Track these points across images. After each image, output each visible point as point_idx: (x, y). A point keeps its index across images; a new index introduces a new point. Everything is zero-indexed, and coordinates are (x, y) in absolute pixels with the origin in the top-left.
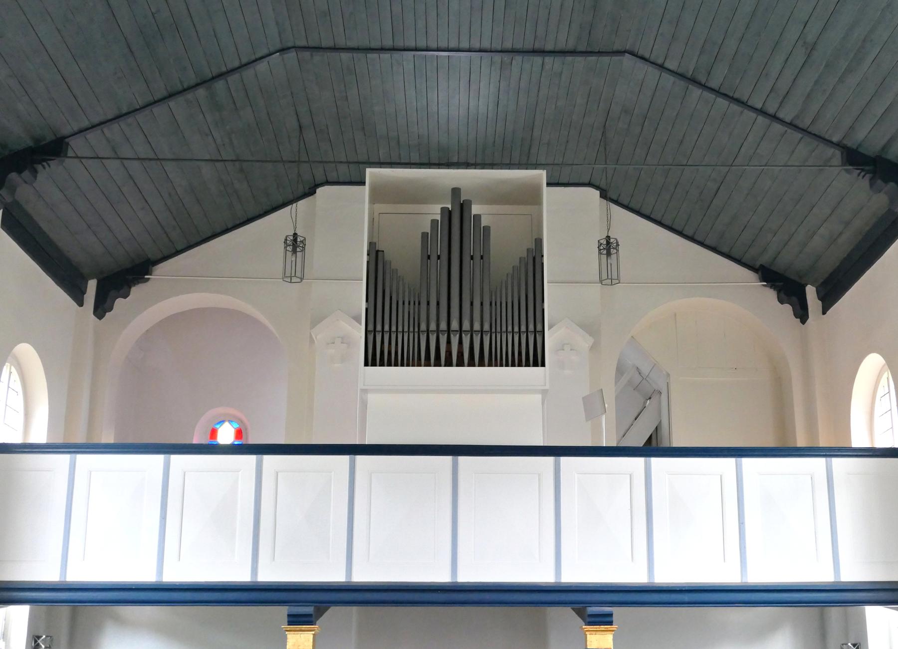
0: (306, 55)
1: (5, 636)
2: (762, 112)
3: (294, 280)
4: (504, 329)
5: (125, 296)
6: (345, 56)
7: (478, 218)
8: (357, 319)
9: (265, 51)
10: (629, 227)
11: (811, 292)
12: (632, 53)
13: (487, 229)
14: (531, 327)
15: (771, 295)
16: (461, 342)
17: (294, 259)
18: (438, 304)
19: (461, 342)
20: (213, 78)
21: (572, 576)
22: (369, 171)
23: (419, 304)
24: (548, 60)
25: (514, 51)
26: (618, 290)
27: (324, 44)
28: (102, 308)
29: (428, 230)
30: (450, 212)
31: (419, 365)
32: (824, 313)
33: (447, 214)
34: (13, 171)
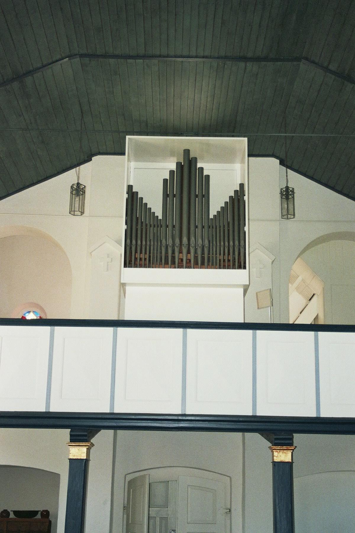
0: (87, 60)
6: (112, 61)
7: (202, 169)
8: (119, 243)
9: (58, 57)
10: (298, 182)
12: (307, 59)
13: (208, 177)
20: (24, 74)
21: (265, 410)
22: (127, 137)
24: (249, 65)
25: (226, 57)
26: (290, 224)
27: (98, 53)
29: (168, 177)
34: (28, 320)
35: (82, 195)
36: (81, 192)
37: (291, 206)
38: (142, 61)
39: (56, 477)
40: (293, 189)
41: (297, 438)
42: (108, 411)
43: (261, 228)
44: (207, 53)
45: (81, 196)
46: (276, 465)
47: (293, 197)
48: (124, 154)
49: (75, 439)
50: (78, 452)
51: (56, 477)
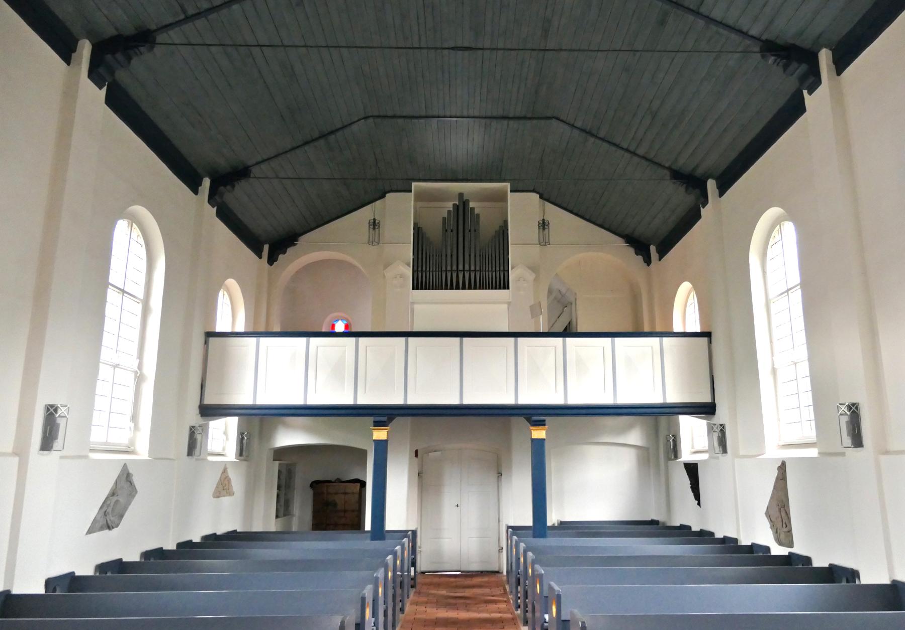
0: (379, 120)
2: (627, 150)
5: (284, 253)
6: (400, 121)
7: (473, 209)
8: (408, 265)
10: (555, 214)
11: (653, 249)
13: (478, 215)
14: (502, 268)
15: (631, 251)
21: (524, 400)
22: (414, 184)
24: (511, 122)
28: (272, 260)
29: (446, 215)
33: (456, 207)
41: (548, 419)
44: (477, 114)
48: (410, 191)
49: (378, 424)
50: (380, 434)
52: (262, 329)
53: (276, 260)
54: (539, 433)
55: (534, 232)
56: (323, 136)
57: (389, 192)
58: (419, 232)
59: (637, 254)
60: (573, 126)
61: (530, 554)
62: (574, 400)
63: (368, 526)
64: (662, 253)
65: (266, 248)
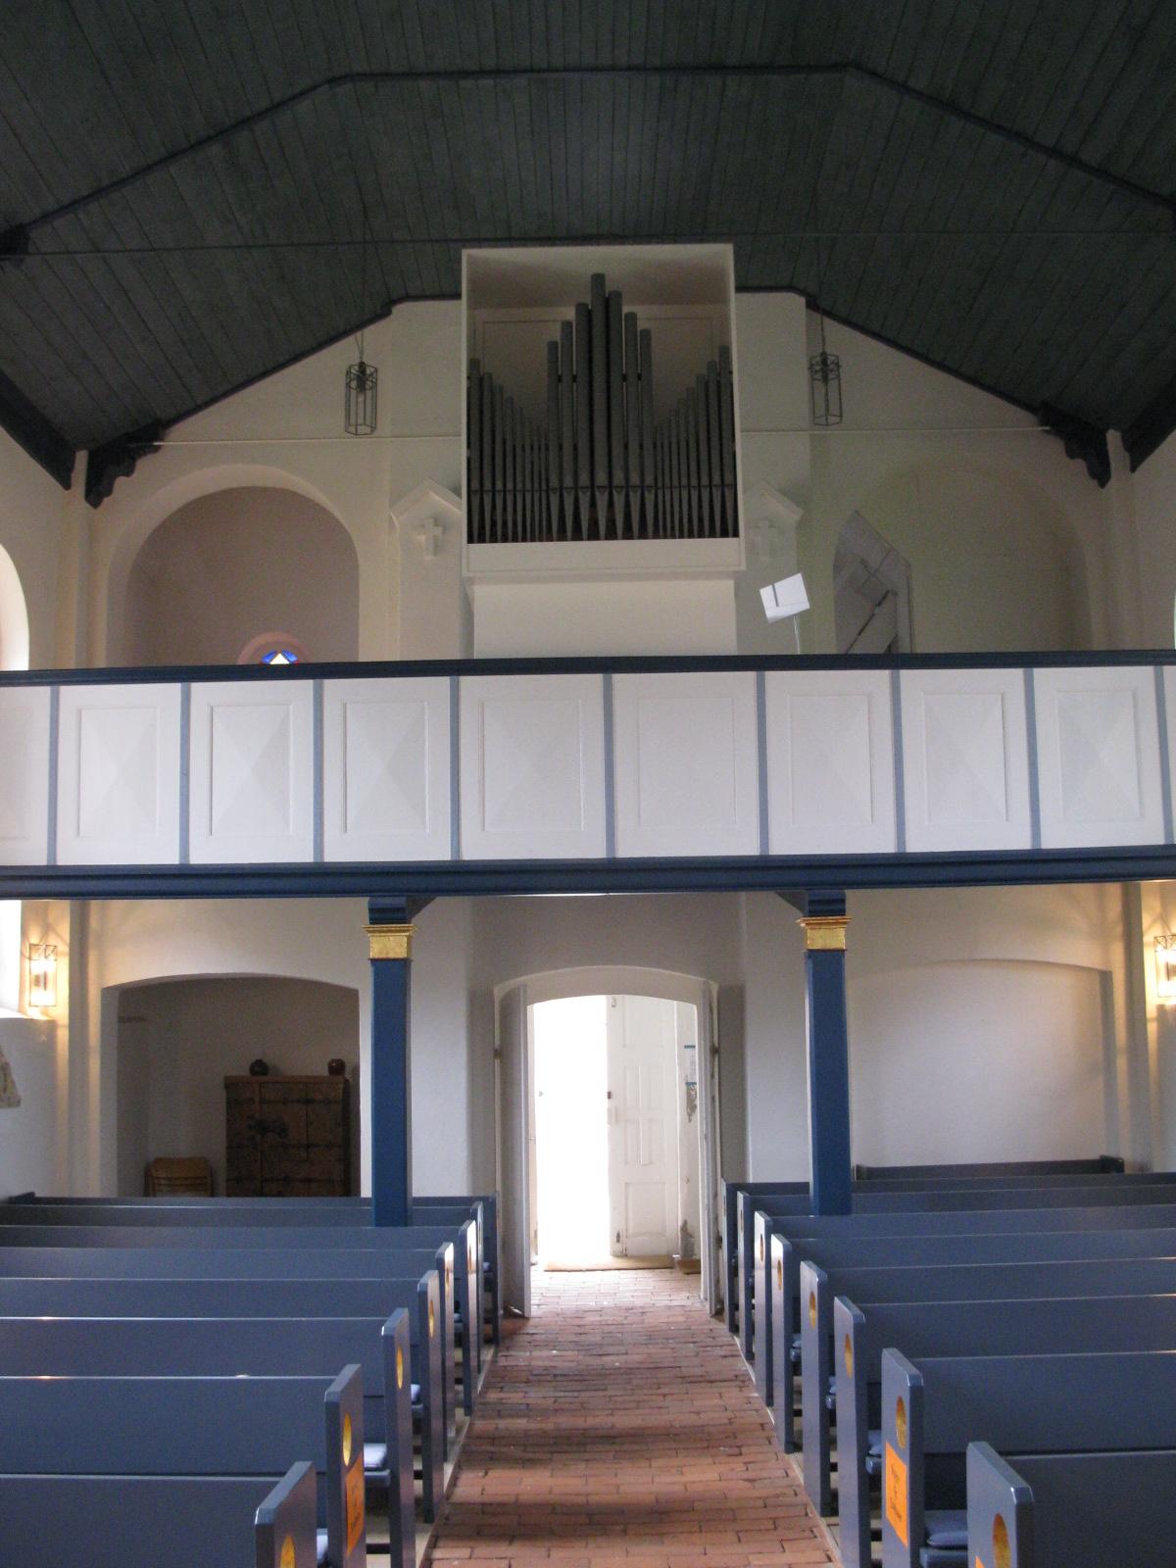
1: (790, 1565)
2: (1054, 152)
3: (362, 429)
4: (676, 483)
5: (129, 472)
6: (423, 85)
7: (632, 317)
8: (457, 491)
11: (1113, 439)
13: (646, 333)
14: (717, 479)
15: (1055, 447)
16: (611, 504)
17: (361, 399)
18: (575, 448)
19: (611, 504)
20: (233, 126)
21: (787, 843)
22: (467, 254)
23: (547, 449)
25: (680, 69)
28: (96, 492)
29: (557, 336)
30: (590, 313)
31: (550, 539)
32: (1133, 469)
33: (585, 313)
35: (371, 388)
36: (370, 384)
37: (833, 395)
38: (491, 81)
39: (351, 996)
40: (837, 357)
41: (852, 896)
42: (448, 858)
43: (763, 457)
45: (369, 393)
46: (814, 955)
47: (838, 377)
49: (382, 917)
50: (390, 944)
51: (351, 996)
52: (71, 663)
53: (109, 492)
54: (829, 936)
55: (795, 387)
56: (222, 133)
57: (408, 297)
58: (483, 395)
59: (1071, 454)
60: (904, 88)
61: (844, 1313)
62: (927, 839)
63: (366, 1190)
64: (1141, 447)
65: (81, 459)
